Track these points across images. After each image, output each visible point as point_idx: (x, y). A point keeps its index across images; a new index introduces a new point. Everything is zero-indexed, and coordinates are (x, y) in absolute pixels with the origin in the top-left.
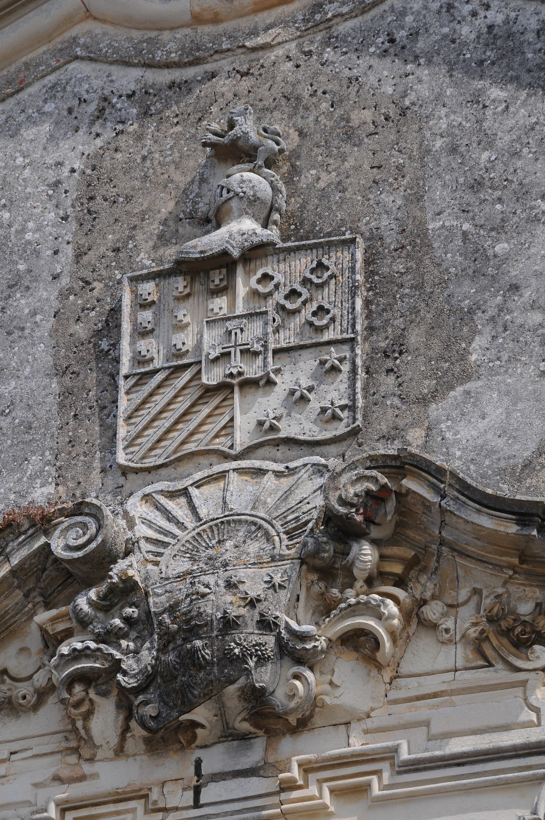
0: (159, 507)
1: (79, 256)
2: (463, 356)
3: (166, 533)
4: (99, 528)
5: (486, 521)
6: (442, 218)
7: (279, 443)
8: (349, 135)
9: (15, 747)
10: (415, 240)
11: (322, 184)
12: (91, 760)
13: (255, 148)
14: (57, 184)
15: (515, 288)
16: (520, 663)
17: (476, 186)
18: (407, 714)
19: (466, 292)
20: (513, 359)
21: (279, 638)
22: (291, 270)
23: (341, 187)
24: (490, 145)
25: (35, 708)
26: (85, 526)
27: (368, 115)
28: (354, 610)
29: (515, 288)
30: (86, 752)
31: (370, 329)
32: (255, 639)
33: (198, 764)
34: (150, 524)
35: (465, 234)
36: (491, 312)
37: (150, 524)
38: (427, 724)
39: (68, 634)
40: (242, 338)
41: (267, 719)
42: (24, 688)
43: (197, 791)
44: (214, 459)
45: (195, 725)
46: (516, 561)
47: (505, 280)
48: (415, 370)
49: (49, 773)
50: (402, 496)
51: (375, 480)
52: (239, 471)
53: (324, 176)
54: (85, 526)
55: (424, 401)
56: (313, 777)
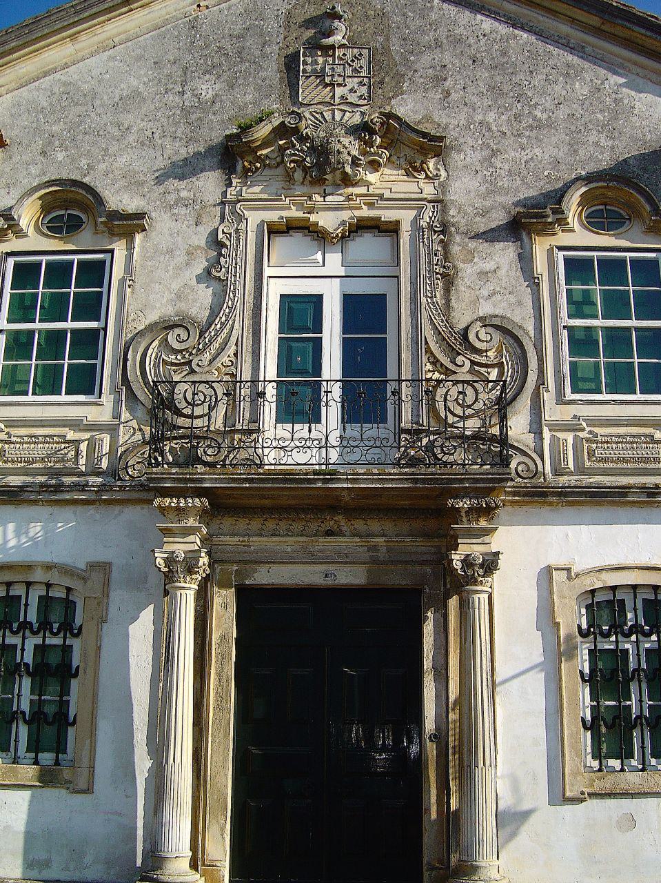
0: (313, 116)
1: (285, 38)
2: (402, 87)
3: (320, 122)
4: (299, 122)
5: (413, 136)
6: (394, 48)
7: (347, 103)
8: (367, 17)
9: (271, 177)
10: (386, 51)
11: (359, 30)
12: (293, 184)
13: (342, 16)
14: (278, 16)
15: (416, 71)
16: (418, 176)
17: (405, 39)
18: (385, 185)
19: (402, 70)
20: (416, 91)
21: (352, 158)
22: (349, 53)
23: (364, 31)
24: (409, 29)
25: (276, 167)
26: (296, 119)
27: (372, 13)
28: (373, 154)
29: (416, 71)
30: (292, 182)
31: (374, 75)
32: (346, 158)
33: (325, 190)
34: (311, 120)
35: (402, 53)
36: (409, 76)
37: (311, 120)
38: (391, 189)
39: (288, 148)
40: (338, 71)
41: (347, 181)
42: (273, 162)
43: (324, 197)
44: (328, 105)
45: (326, 179)
46: (419, 148)
47: (414, 68)
48: (388, 88)
49: (280, 187)
50: (389, 124)
51: (383, 119)
52: (339, 109)
53: (359, 27)
54: (296, 119)
55: (390, 99)
56: (288, 199)
